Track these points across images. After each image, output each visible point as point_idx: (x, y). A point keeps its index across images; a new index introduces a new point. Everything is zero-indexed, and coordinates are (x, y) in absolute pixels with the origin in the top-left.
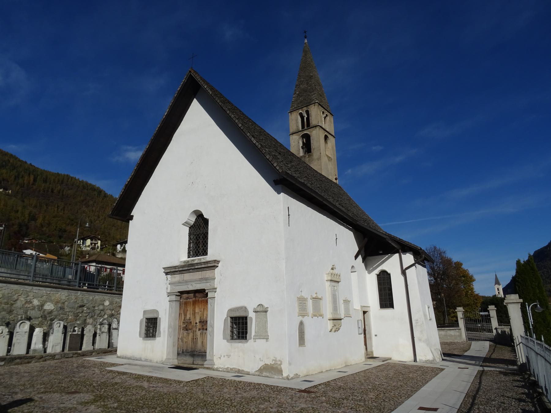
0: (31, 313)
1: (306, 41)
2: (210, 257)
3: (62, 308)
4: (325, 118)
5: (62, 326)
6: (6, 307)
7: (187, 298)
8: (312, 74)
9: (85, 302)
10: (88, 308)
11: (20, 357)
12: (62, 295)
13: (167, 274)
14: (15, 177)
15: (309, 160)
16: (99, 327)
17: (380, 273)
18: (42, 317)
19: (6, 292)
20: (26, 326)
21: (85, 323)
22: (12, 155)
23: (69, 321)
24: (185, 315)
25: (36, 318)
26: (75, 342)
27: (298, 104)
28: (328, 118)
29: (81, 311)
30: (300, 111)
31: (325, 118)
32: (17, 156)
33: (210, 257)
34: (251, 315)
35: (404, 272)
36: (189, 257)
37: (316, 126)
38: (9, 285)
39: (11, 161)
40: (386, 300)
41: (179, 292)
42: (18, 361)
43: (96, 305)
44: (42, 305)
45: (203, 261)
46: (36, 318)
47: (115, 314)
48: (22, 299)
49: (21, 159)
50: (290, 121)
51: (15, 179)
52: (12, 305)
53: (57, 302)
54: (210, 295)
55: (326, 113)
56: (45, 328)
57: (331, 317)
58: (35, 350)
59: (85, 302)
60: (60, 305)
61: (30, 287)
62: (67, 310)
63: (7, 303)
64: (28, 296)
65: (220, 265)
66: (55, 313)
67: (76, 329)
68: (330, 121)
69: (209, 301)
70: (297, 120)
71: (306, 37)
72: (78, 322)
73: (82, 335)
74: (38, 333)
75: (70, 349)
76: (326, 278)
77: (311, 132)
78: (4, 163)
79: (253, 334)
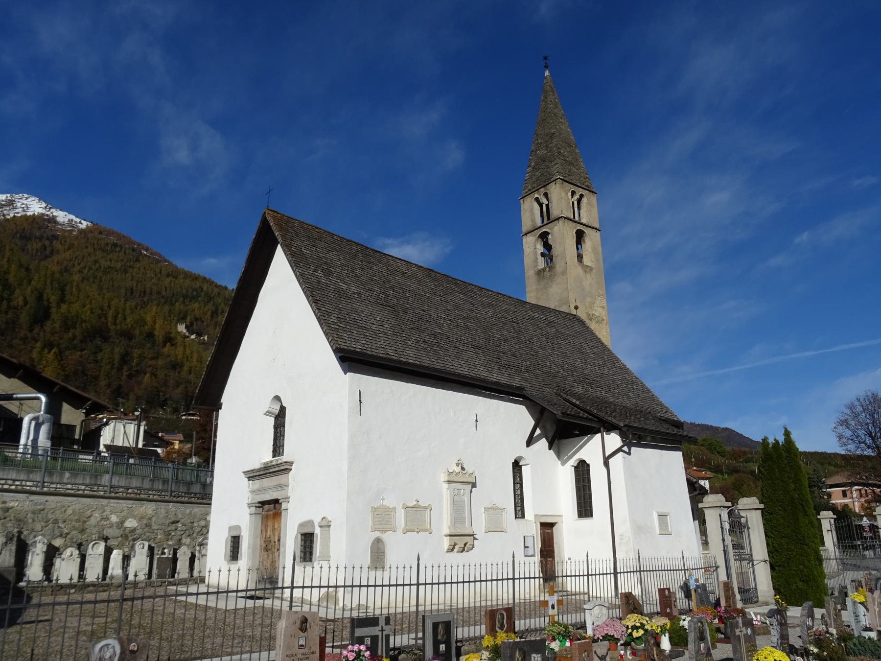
0: (108, 532)
1: (547, 73)
2: (285, 458)
3: (148, 525)
4: (579, 201)
5: (146, 547)
6: (77, 525)
7: (268, 510)
8: (553, 131)
9: (180, 516)
10: (184, 525)
11: (93, 585)
12: (149, 508)
13: (249, 478)
14: (212, 313)
15: (551, 276)
16: (198, 548)
17: (578, 464)
18: (121, 536)
19: (77, 507)
20: (101, 548)
21: (179, 543)
22: (205, 278)
23: (157, 540)
24: (266, 532)
25: (114, 538)
26: (165, 567)
27: (534, 183)
28: (584, 200)
29: (174, 528)
30: (536, 196)
31: (579, 201)
32: (213, 279)
33: (285, 458)
34: (317, 531)
35: (606, 464)
36: (274, 456)
37: (558, 219)
38: (80, 499)
39: (205, 289)
40: (585, 509)
41: (259, 502)
42: (91, 588)
43: (195, 520)
44: (122, 522)
45: (280, 462)
46: (114, 538)
47: (204, 531)
48: (97, 515)
49: (219, 283)
50: (523, 212)
51: (212, 316)
52: (85, 522)
53: (142, 518)
54: (284, 506)
55: (579, 191)
56: (126, 550)
57: (447, 532)
58: (112, 578)
59: (180, 516)
60: (145, 521)
61: (106, 501)
62: (155, 527)
63: (78, 521)
64: (104, 511)
65: (293, 467)
66: (139, 531)
67: (166, 551)
68: (589, 204)
69: (283, 513)
70: (532, 210)
71: (546, 67)
72: (170, 543)
73: (175, 560)
74: (116, 556)
75: (159, 576)
76: (443, 480)
77: (551, 229)
78: (195, 293)
79: (318, 554)
